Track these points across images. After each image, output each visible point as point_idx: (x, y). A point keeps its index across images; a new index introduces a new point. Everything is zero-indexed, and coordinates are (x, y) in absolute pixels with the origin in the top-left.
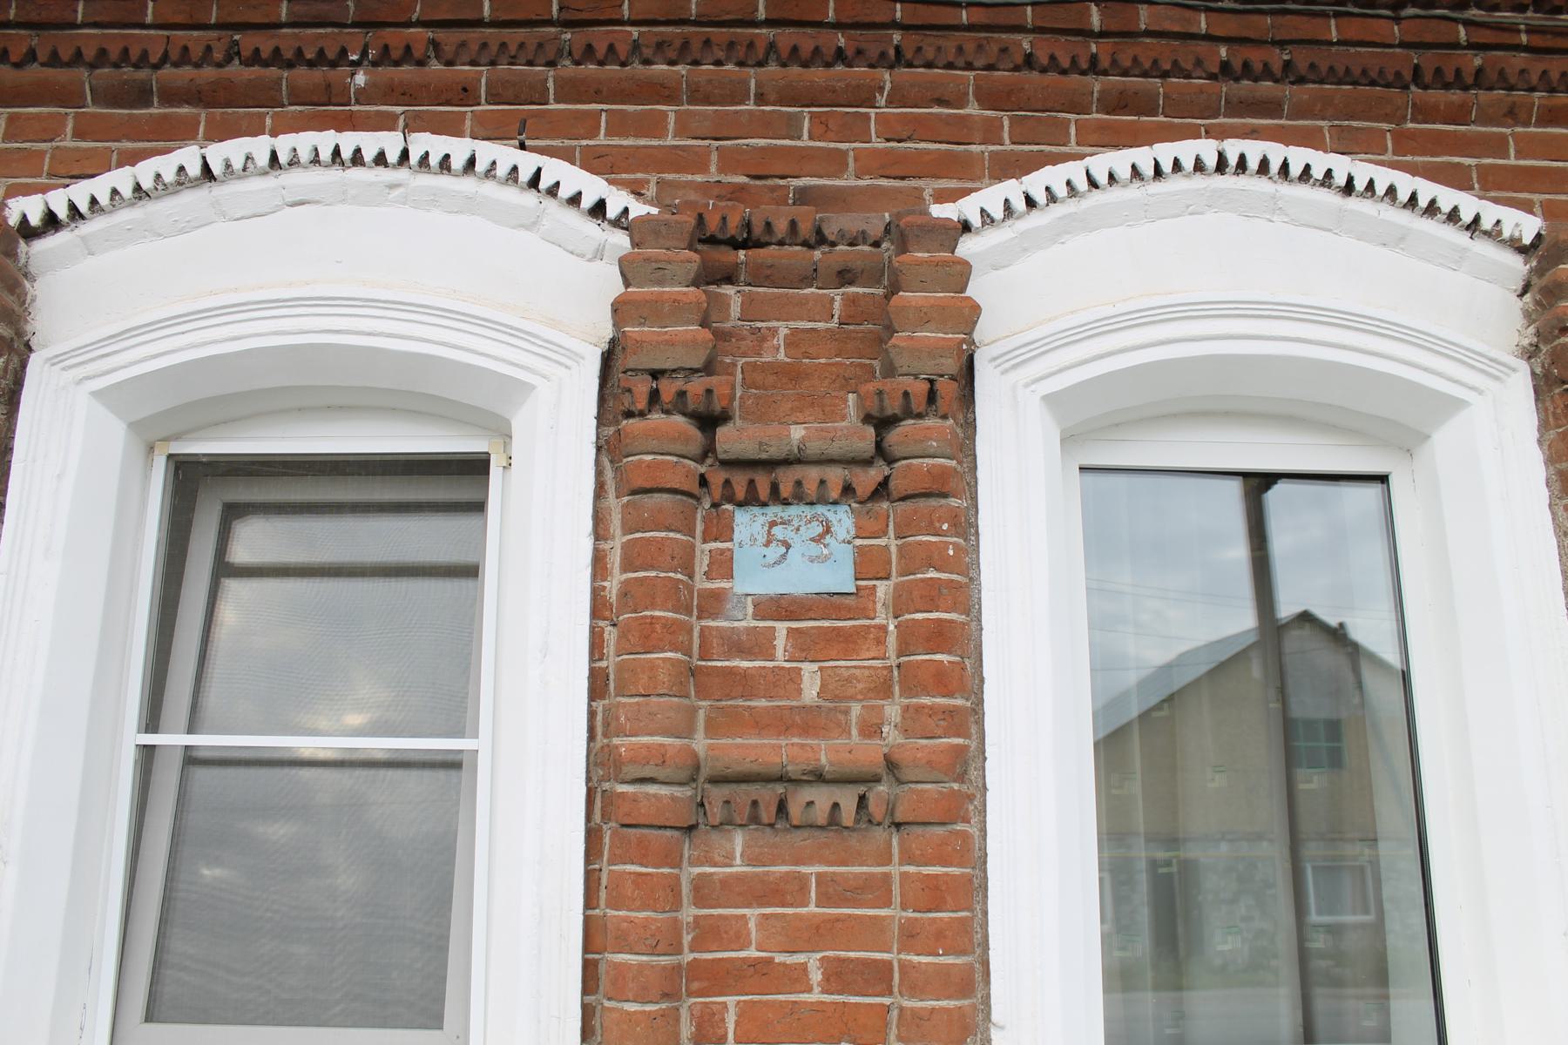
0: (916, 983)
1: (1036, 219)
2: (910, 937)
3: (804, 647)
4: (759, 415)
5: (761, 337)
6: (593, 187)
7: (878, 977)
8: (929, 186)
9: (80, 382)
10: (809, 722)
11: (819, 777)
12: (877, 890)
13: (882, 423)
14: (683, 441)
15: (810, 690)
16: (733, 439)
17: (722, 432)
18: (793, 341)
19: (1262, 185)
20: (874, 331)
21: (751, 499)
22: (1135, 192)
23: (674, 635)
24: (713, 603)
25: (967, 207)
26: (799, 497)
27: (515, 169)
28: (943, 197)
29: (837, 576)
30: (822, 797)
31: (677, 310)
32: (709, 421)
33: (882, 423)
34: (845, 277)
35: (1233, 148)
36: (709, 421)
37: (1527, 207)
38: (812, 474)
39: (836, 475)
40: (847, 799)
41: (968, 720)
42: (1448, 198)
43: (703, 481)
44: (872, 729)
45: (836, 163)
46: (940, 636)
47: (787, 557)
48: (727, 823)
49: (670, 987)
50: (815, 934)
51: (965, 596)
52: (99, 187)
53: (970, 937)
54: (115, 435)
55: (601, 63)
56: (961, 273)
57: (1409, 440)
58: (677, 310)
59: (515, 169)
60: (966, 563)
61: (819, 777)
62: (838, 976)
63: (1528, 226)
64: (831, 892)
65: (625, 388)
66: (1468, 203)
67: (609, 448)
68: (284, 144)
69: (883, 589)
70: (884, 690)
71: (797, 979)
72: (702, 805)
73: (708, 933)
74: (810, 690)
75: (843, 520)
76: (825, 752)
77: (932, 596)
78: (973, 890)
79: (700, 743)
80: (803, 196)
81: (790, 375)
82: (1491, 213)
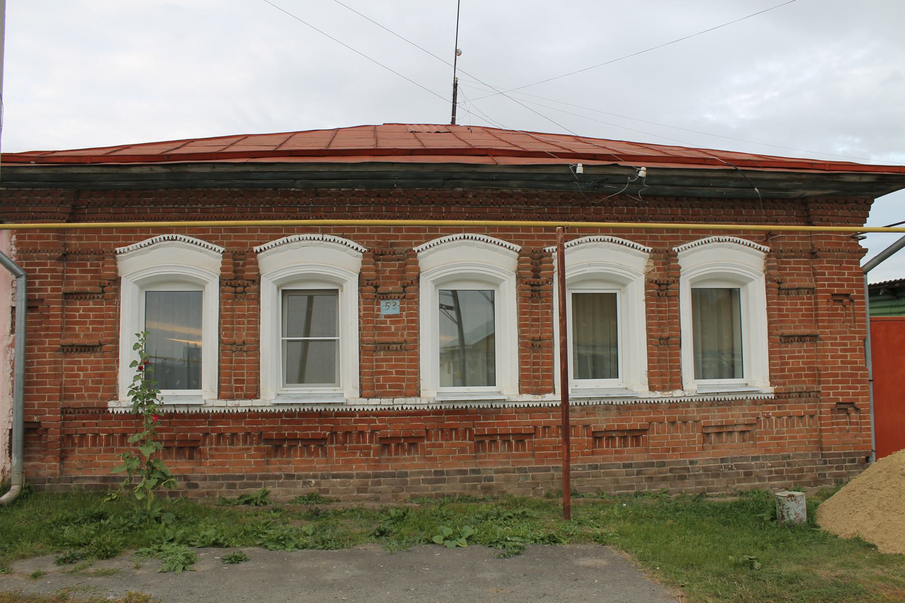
0: (409, 373)
1: (431, 249)
2: (408, 367)
3: (392, 322)
4: (385, 284)
5: (385, 271)
6: (356, 245)
7: (403, 373)
8: (413, 241)
10: (393, 334)
11: (394, 343)
12: (403, 360)
13: (404, 287)
14: (371, 289)
15: (393, 329)
16: (380, 290)
17: (379, 289)
18: (390, 271)
19: (472, 241)
20: (403, 270)
21: (383, 299)
22: (449, 243)
23: (372, 322)
24: (378, 316)
25: (420, 248)
26: (391, 298)
28: (417, 244)
29: (397, 312)
30: (395, 346)
31: (371, 270)
32: (376, 287)
33: (404, 287)
34: (399, 260)
35: (467, 235)
36: (376, 287)
37: (519, 244)
38: (393, 295)
39: (397, 295)
40: (399, 346)
41: (417, 334)
42: (505, 243)
44: (402, 336)
45: (397, 237)
46: (413, 321)
47: (390, 308)
48: (380, 350)
49: (372, 374)
50: (394, 366)
51: (417, 315)
52: (266, 245)
53: (417, 367)
56: (417, 262)
57: (498, 286)
58: (371, 270)
60: (418, 309)
61: (394, 343)
62: (397, 373)
63: (518, 248)
64: (396, 360)
65: (363, 282)
66: (508, 244)
67: (360, 291)
68: (301, 236)
69: (404, 313)
70: (404, 329)
71: (391, 373)
72: (545, 595)
73: (378, 367)
74: (393, 329)
75: (398, 302)
76: (395, 339)
77: (412, 315)
78: (418, 360)
79: (376, 338)
80: (392, 245)
81: (389, 278)
82: (512, 245)
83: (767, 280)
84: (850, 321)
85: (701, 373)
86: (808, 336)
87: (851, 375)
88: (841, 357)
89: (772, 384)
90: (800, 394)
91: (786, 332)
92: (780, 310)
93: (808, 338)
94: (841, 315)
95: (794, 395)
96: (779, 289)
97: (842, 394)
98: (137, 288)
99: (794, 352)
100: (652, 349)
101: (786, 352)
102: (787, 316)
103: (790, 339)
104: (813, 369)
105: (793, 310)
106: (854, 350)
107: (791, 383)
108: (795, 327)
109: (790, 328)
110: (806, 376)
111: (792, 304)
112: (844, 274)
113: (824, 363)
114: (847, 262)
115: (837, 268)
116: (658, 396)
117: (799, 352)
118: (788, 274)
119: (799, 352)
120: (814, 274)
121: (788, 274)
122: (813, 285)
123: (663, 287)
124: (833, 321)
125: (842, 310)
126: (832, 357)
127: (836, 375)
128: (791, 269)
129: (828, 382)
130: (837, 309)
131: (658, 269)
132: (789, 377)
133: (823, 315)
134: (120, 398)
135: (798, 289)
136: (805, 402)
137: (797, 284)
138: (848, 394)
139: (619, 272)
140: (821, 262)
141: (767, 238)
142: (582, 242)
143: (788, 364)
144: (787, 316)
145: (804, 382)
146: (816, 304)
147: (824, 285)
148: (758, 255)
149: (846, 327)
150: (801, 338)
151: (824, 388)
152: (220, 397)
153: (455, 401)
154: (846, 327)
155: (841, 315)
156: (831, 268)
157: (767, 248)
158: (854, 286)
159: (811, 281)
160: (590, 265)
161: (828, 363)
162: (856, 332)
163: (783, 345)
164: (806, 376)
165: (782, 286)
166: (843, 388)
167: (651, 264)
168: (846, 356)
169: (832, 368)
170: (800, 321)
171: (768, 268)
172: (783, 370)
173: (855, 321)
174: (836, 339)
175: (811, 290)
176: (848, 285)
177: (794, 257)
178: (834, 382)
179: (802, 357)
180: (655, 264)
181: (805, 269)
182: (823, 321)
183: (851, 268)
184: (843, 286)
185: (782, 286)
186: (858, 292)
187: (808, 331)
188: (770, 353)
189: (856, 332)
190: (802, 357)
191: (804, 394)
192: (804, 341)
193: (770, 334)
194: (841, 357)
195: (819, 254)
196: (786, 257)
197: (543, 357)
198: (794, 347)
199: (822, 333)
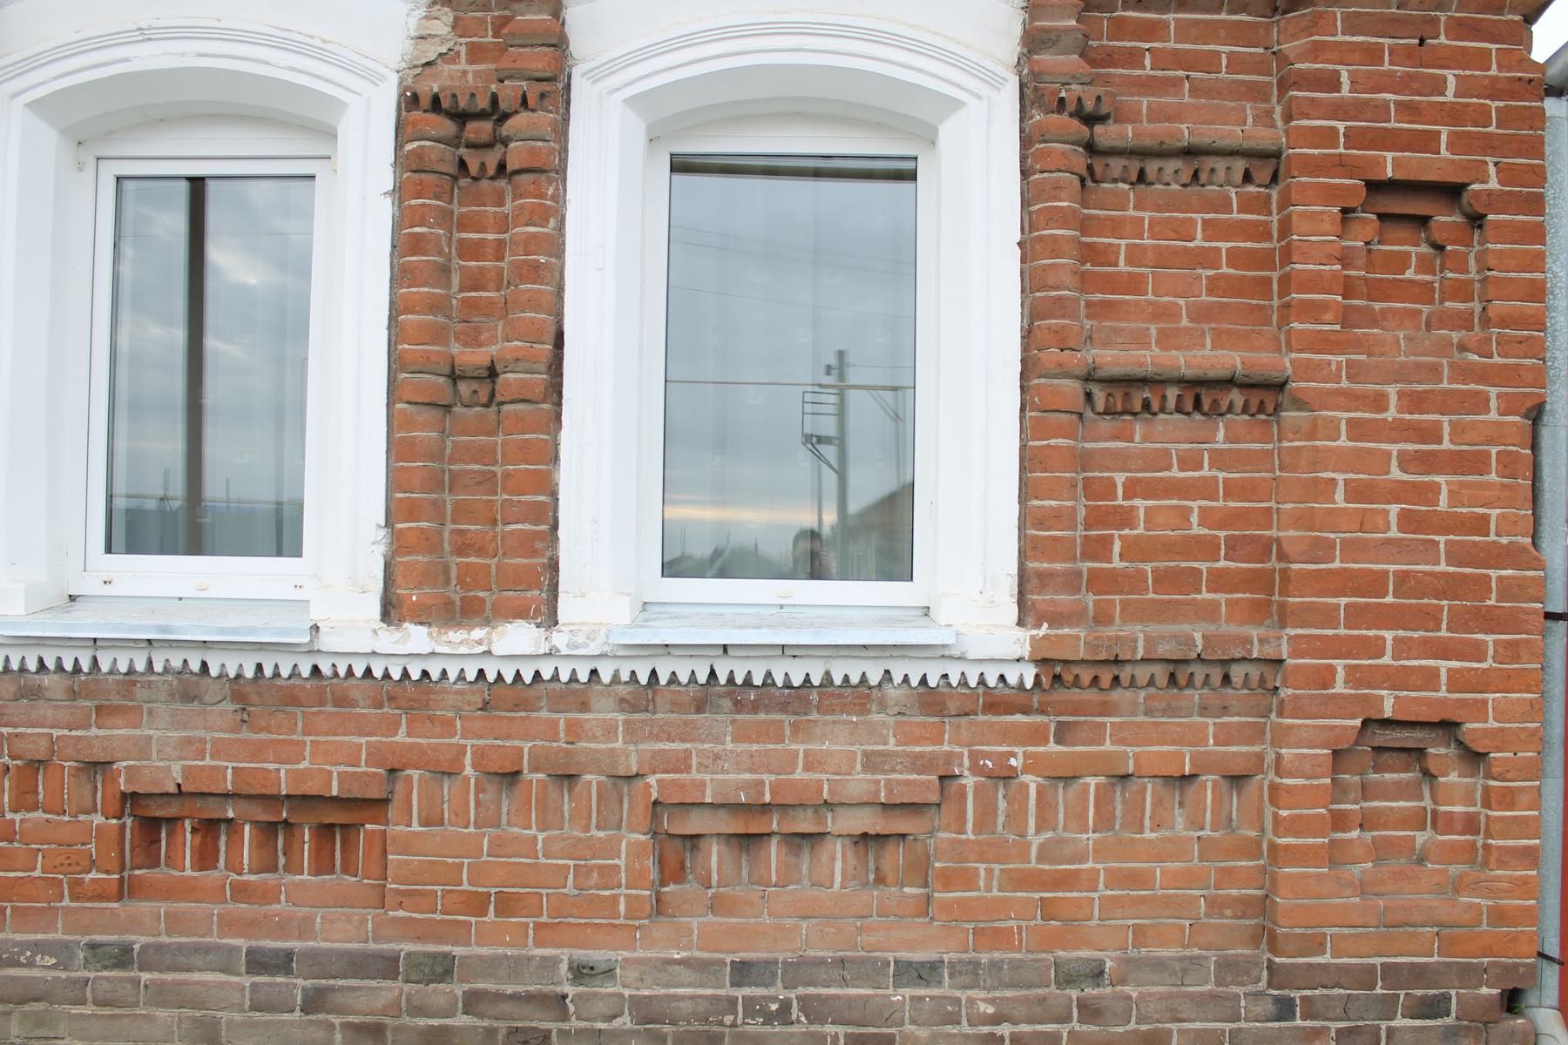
43: (462, 164)
54: (638, 130)
152: (391, 611)
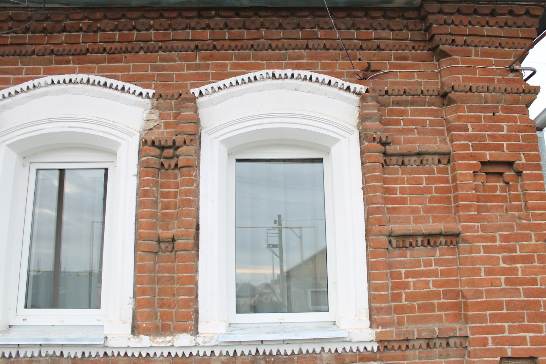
9: (3, 142)
27: (231, 83)
43: (162, 164)
55: (239, 50)
59: (231, 83)
83: (362, 139)
84: (519, 209)
85: (406, 300)
86: (440, 235)
87: (526, 305)
88: (503, 271)
89: (373, 323)
90: (429, 343)
91: (399, 228)
92: (387, 191)
93: (443, 240)
94: (503, 199)
95: (417, 344)
96: (385, 154)
97: (511, 341)
98: (14, 156)
99: (417, 264)
100: (142, 259)
101: (403, 265)
102: (403, 201)
103: (408, 241)
104: (456, 294)
105: (412, 191)
106: (529, 259)
107: (411, 321)
108: (416, 220)
109: (408, 221)
110: (442, 307)
111: (410, 181)
112: (501, 129)
113: (472, 283)
114: (505, 110)
115: (486, 119)
116: (144, 343)
117: (428, 264)
118: (402, 132)
119: (428, 264)
120: (449, 130)
121: (402, 132)
122: (444, 148)
123: (169, 152)
124: (488, 210)
125: (503, 190)
126: (488, 272)
127: (499, 306)
128: (406, 123)
129: (483, 319)
130: (495, 189)
131: (167, 125)
132: (411, 309)
133: (466, 198)
134: (202, 327)
135: (419, 154)
136: (440, 357)
137: (417, 147)
138: (523, 340)
139: (97, 130)
140: (458, 110)
141: (366, 74)
142: (40, 86)
143: (406, 286)
144: (403, 201)
145: (439, 319)
146: (454, 179)
147: (466, 147)
148: (136, 104)
149: (513, 218)
150: (430, 239)
151: (474, 331)
152: (135, 330)
153: (240, 343)
154: (513, 218)
155: (503, 199)
156: (478, 119)
157: (361, 88)
158: (520, 148)
159: (444, 141)
160: (50, 121)
161: (481, 282)
162: (529, 227)
163: (397, 252)
164: (442, 307)
165: (390, 149)
166: (512, 329)
167: (155, 117)
168: (514, 271)
169: (489, 293)
170: (427, 210)
171: (363, 118)
172: (397, 297)
173: (527, 209)
174: (493, 239)
175: (445, 157)
176: (509, 147)
177: (412, 103)
178: (493, 318)
179: (433, 273)
180: (161, 116)
181: (432, 123)
182: (467, 208)
183: (514, 120)
184: (500, 148)
185: (390, 149)
186: (527, 157)
187: (440, 227)
188: (370, 266)
189: (529, 227)
190: (433, 273)
191: (438, 342)
192: (435, 245)
193: (368, 233)
194: (503, 271)
195: (452, 95)
196: (398, 103)
197: (463, 262)
198: (418, 255)
199: (467, 229)
